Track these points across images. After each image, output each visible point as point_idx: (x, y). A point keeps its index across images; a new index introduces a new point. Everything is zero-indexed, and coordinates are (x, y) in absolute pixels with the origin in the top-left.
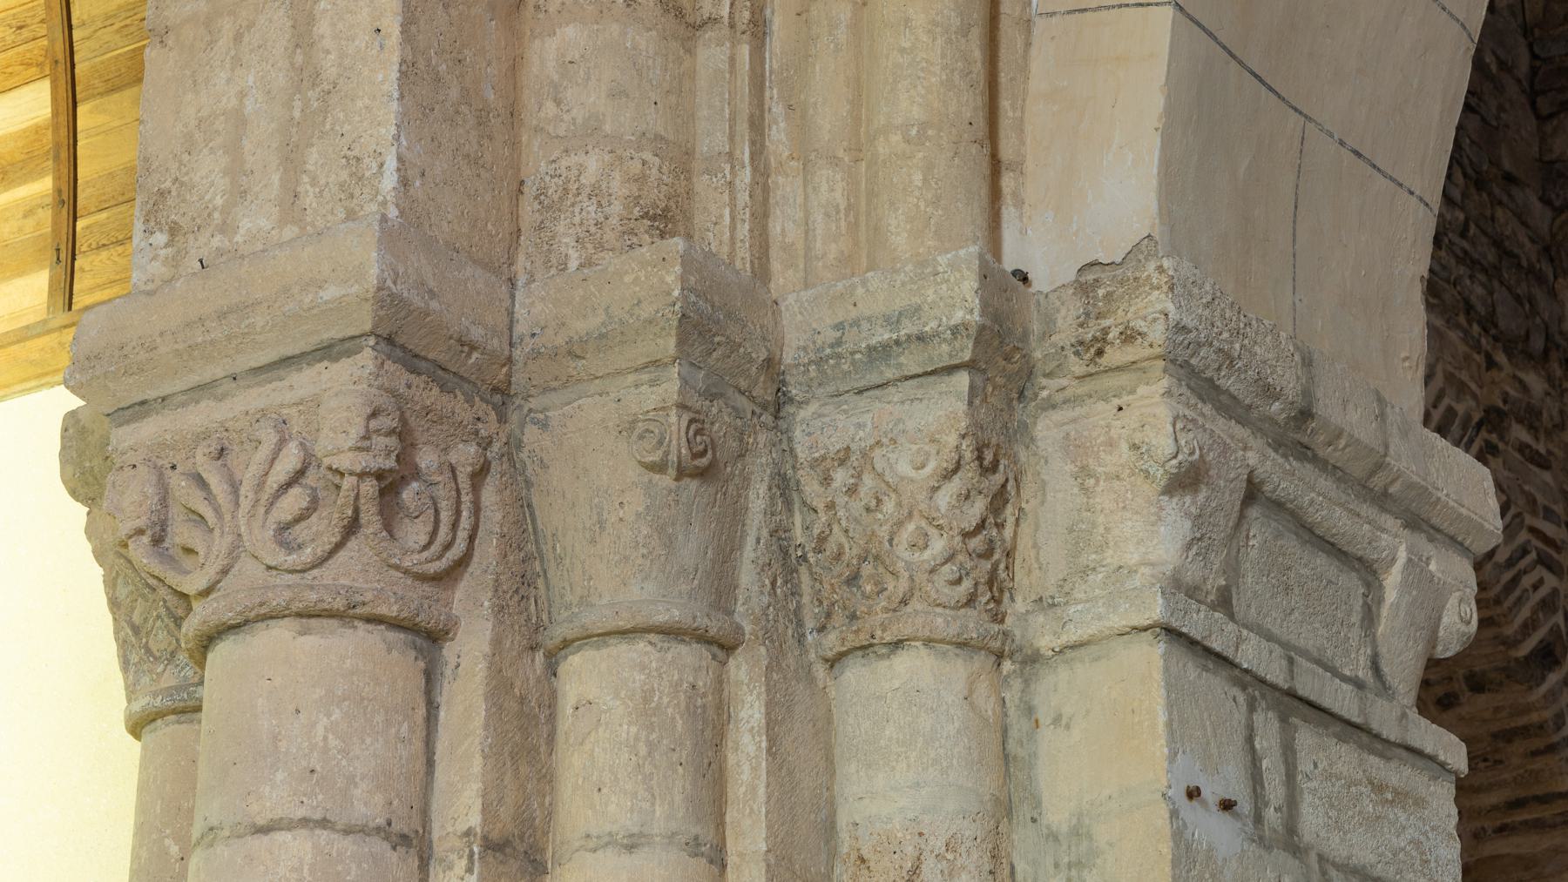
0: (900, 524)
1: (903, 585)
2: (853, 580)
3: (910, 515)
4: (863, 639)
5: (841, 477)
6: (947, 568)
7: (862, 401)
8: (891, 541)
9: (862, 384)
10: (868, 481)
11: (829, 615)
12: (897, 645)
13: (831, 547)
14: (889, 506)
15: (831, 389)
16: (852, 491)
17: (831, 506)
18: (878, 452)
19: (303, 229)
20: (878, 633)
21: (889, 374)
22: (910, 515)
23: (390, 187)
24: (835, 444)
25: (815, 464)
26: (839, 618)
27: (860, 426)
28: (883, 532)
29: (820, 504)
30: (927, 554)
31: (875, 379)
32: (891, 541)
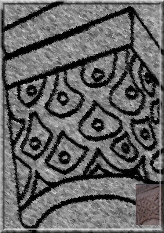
0: (150, 205)
1: (151, 212)
2: (144, 213)
3: (152, 204)
4: (146, 219)
5: (142, 202)
6: (157, 210)
7: (145, 193)
8: (149, 207)
9: (145, 191)
10: (146, 201)
11: (141, 218)
12: (151, 219)
13: (141, 210)
14: (149, 203)
15: (141, 192)
16: (144, 202)
17: (141, 205)
18: (147, 198)
19: (107, 209)
20: (148, 218)
21: (149, 189)
22: (152, 204)
23: (64, 159)
24: (142, 198)
25: (139, 200)
26: (143, 217)
27: (145, 195)
28: (149, 206)
29: (140, 205)
30: (154, 208)
31: (147, 190)
32: (149, 207)
